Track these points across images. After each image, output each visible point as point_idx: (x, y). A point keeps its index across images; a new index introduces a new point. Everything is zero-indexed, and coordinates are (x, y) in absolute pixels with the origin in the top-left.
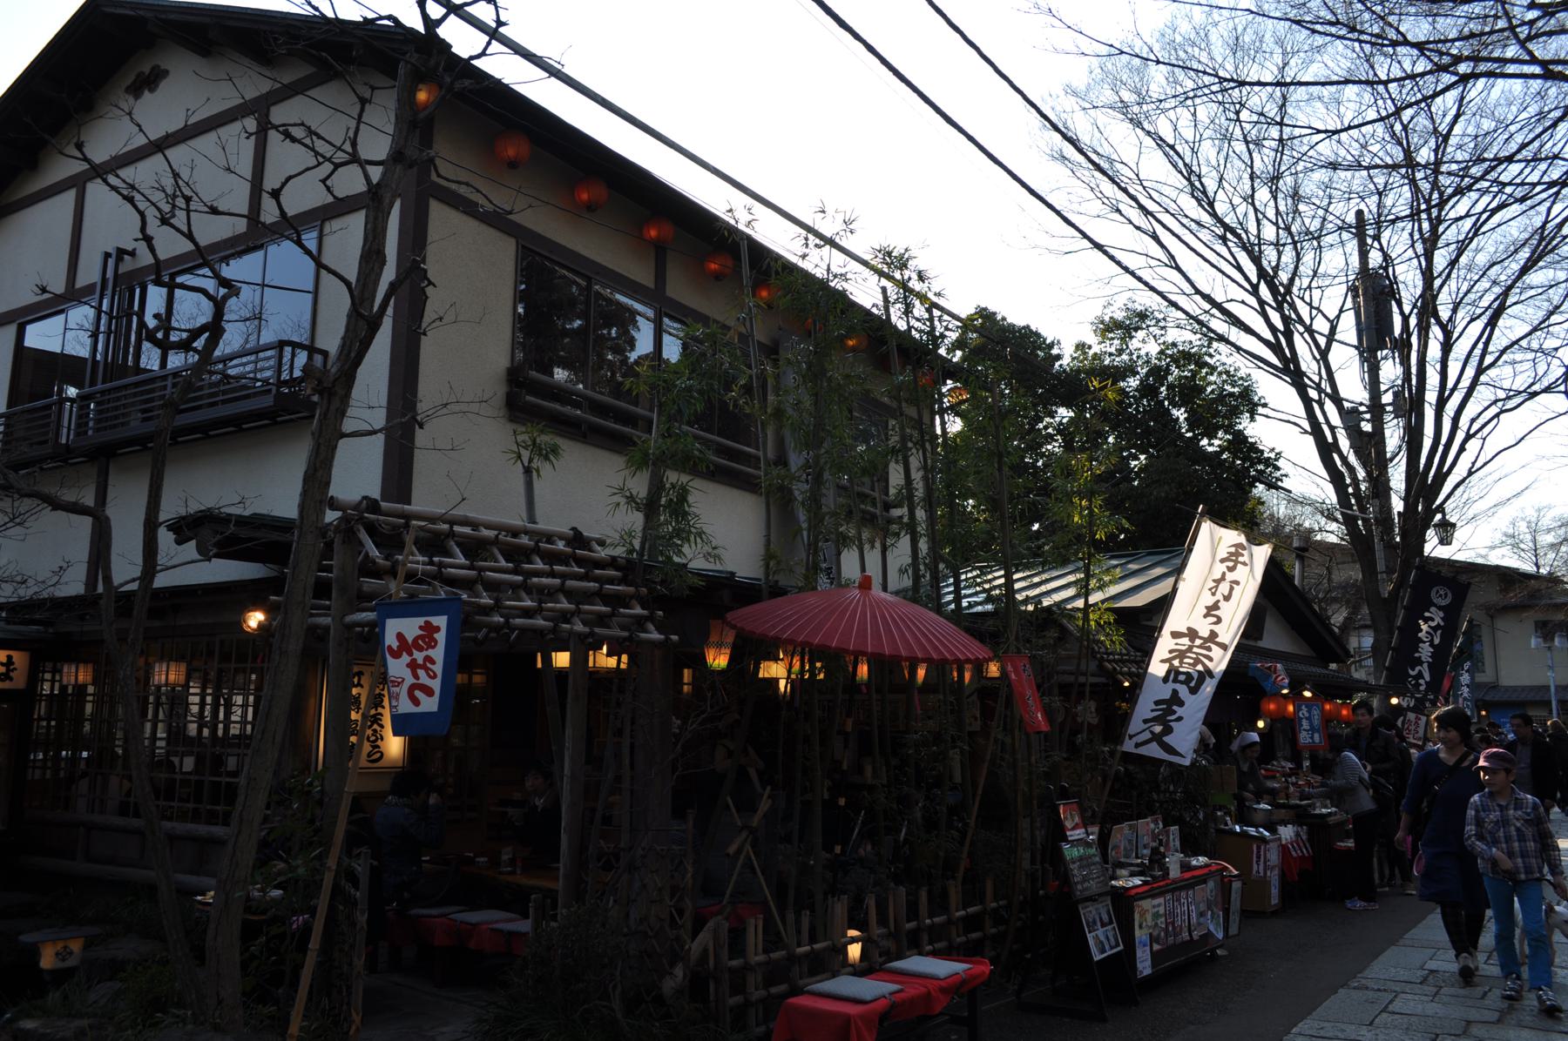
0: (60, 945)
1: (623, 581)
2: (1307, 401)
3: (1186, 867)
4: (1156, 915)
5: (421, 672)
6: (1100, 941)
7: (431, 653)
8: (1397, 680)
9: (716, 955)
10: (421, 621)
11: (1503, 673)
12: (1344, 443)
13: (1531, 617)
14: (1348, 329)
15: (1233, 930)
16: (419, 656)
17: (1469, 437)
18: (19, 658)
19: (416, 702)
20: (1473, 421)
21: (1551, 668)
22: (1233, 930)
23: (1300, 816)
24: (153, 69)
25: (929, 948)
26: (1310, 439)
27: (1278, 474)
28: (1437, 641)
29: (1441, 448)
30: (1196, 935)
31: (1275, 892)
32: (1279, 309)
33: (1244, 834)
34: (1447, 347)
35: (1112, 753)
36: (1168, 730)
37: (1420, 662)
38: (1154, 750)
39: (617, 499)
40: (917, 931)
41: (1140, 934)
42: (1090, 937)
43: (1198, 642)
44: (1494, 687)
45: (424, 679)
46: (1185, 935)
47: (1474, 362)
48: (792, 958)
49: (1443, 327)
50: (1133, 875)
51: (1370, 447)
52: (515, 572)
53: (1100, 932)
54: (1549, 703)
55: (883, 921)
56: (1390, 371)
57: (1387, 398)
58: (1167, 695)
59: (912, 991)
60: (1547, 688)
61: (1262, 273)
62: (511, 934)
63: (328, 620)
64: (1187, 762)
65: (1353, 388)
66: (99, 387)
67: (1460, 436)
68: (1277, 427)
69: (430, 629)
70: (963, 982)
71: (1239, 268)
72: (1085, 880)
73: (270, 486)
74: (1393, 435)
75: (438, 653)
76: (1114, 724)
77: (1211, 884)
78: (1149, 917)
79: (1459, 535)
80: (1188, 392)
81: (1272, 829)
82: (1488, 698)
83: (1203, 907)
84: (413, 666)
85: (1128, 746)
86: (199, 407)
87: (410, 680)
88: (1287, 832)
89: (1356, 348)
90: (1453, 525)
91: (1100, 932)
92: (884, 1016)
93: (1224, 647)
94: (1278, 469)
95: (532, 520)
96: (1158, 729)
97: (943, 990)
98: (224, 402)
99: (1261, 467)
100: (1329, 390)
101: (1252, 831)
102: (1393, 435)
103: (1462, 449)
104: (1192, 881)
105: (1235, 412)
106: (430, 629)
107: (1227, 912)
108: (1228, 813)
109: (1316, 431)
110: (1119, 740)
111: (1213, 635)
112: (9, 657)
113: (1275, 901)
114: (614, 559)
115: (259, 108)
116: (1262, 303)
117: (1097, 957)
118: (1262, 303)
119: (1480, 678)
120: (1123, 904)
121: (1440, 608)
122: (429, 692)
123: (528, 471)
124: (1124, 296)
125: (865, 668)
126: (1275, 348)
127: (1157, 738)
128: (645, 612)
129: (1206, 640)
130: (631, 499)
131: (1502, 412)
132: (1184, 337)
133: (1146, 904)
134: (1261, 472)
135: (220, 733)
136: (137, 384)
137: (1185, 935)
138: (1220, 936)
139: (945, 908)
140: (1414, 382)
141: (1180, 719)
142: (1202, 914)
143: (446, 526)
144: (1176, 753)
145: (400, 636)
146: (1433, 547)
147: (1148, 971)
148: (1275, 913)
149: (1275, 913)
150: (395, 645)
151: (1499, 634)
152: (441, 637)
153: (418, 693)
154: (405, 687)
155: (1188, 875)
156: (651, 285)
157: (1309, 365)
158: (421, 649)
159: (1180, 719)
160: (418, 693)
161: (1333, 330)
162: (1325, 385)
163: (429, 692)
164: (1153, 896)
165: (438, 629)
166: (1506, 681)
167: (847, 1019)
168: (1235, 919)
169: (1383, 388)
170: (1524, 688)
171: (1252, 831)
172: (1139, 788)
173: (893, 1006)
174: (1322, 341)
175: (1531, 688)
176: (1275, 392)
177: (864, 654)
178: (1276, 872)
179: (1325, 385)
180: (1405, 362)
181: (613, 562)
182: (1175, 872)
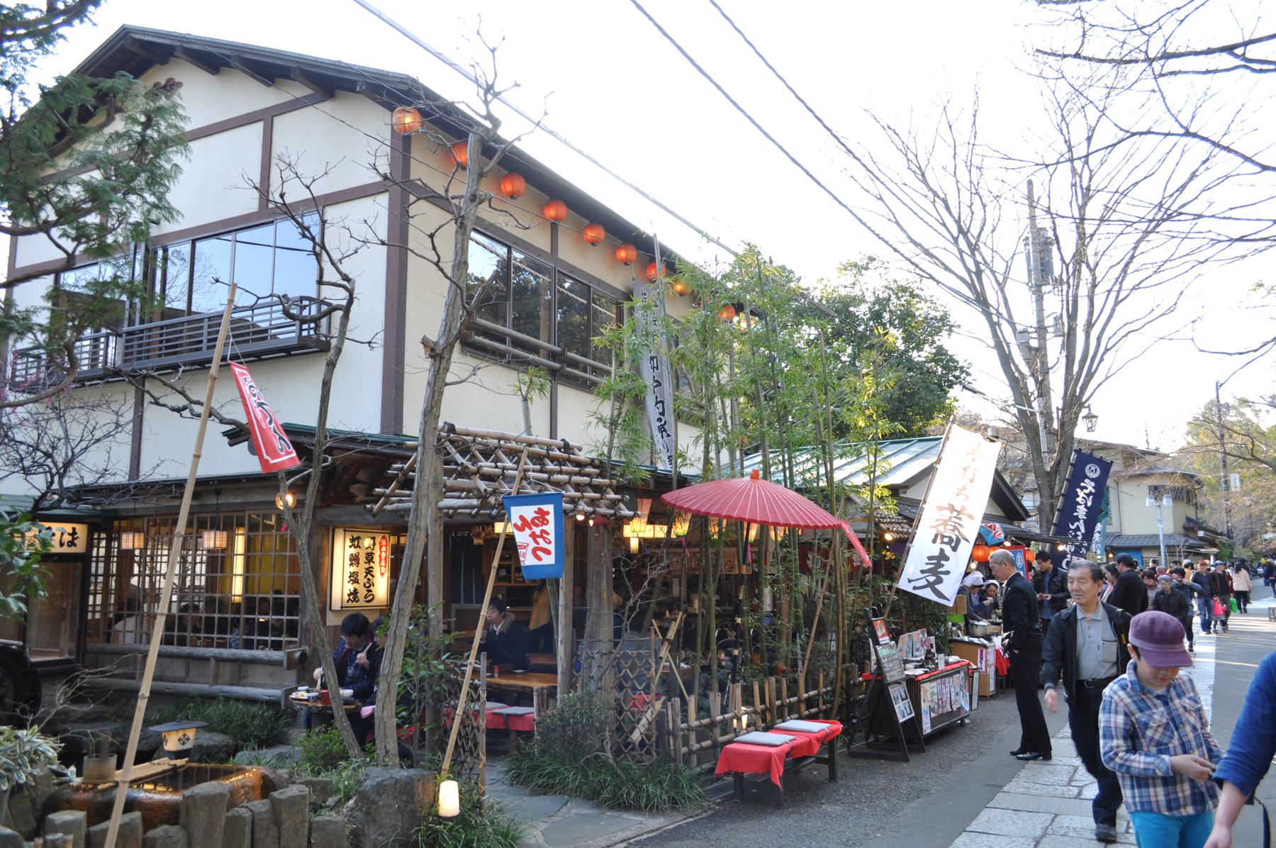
0: (181, 734)
1: (601, 475)
2: (994, 326)
3: (947, 663)
4: (932, 694)
5: (540, 540)
6: (902, 710)
7: (544, 527)
9: (674, 721)
10: (535, 508)
14: (1020, 270)
15: (975, 706)
16: (537, 530)
18: (81, 530)
19: (540, 559)
21: (1160, 521)
24: (168, 80)
25: (806, 713)
26: (995, 352)
28: (1089, 504)
31: (992, 682)
32: (973, 255)
35: (890, 588)
37: (1077, 519)
39: (591, 419)
40: (782, 705)
41: (924, 706)
45: (542, 544)
47: (1113, 295)
49: (1092, 271)
51: (1036, 355)
52: (541, 471)
54: (1159, 547)
55: (763, 701)
59: (801, 740)
61: (961, 230)
62: (508, 715)
63: (410, 504)
65: (1025, 316)
66: (137, 326)
68: (968, 342)
69: (542, 514)
70: (828, 735)
71: (944, 224)
73: (288, 400)
74: (1054, 347)
75: (550, 528)
76: (892, 569)
77: (962, 674)
79: (1099, 424)
80: (905, 318)
81: (989, 639)
82: (1114, 544)
83: (958, 689)
84: (533, 536)
85: (903, 584)
86: (247, 341)
87: (532, 545)
92: (788, 754)
95: (530, 434)
97: (818, 739)
98: (254, 340)
99: (957, 373)
100: (1005, 315)
101: (976, 640)
102: (1054, 347)
103: (1102, 360)
105: (938, 331)
106: (542, 514)
107: (971, 697)
108: (959, 628)
110: (895, 579)
112: (74, 529)
113: (992, 688)
114: (593, 460)
115: (266, 117)
116: (961, 251)
117: (901, 720)
118: (961, 251)
119: (1109, 529)
120: (913, 686)
121: (1092, 480)
122: (548, 552)
123: (525, 399)
124: (860, 245)
126: (971, 286)
130: (600, 419)
132: (904, 276)
134: (957, 378)
135: (188, 583)
136: (190, 322)
138: (967, 708)
142: (957, 694)
143: (496, 441)
145: (522, 518)
146: (1081, 432)
149: (992, 697)
150: (519, 523)
151: (1123, 496)
152: (551, 518)
153: (539, 553)
155: (949, 667)
156: (549, 250)
157: (992, 297)
158: (537, 526)
160: (539, 553)
161: (1008, 268)
162: (1003, 310)
163: (548, 552)
165: (548, 513)
166: (1128, 530)
167: (770, 756)
168: (975, 698)
169: (1046, 314)
170: (1140, 537)
171: (976, 640)
172: (915, 613)
173: (792, 748)
174: (1000, 279)
176: (968, 318)
177: (755, 521)
178: (993, 668)
179: (1003, 310)
181: (592, 463)
182: (942, 667)
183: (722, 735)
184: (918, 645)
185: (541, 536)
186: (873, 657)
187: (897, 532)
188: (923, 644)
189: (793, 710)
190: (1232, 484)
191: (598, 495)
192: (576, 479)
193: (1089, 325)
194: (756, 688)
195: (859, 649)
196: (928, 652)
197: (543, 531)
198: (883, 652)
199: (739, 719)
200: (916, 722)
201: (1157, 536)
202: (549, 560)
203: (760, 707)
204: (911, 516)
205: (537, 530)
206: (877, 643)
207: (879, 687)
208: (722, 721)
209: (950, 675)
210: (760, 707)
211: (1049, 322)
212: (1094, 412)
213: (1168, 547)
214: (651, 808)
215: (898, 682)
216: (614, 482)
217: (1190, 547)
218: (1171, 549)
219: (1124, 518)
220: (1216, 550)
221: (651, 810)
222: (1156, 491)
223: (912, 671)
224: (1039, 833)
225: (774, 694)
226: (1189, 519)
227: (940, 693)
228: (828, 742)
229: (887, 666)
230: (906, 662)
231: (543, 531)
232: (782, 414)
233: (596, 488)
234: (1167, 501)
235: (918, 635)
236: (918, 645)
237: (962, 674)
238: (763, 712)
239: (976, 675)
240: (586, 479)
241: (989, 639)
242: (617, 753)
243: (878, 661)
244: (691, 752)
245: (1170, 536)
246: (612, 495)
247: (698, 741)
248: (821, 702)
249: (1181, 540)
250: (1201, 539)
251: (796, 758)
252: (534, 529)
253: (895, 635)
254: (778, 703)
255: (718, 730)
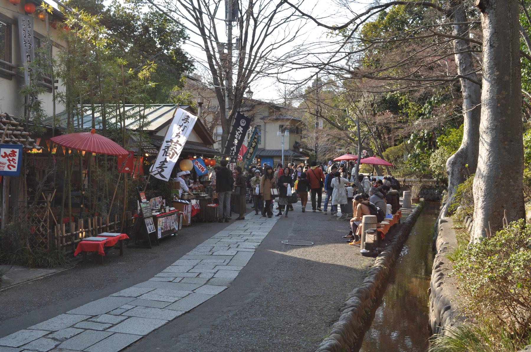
2: (206, 42)
3: (170, 210)
4: (163, 223)
5: (11, 162)
6: (150, 228)
7: (14, 158)
8: (228, 152)
9: (57, 233)
10: (11, 150)
11: (267, 145)
12: (218, 56)
13: (279, 123)
14: (221, 13)
16: (11, 158)
17: (261, 58)
19: (10, 169)
20: (263, 52)
22: (180, 228)
23: (197, 197)
26: (205, 52)
27: (192, 68)
29: (251, 64)
30: (172, 228)
31: (189, 219)
33: (181, 202)
34: (255, 27)
36: (163, 171)
38: (158, 177)
40: (100, 228)
41: (159, 227)
42: (147, 227)
43: (173, 144)
44: (263, 150)
45: (12, 163)
46: (169, 228)
48: (72, 235)
50: (156, 212)
51: (226, 59)
53: (150, 226)
54: (281, 156)
55: (92, 226)
56: (236, 31)
57: (234, 41)
58: (164, 160)
60: (281, 151)
64: (167, 180)
67: (256, 62)
68: (193, 48)
69: (14, 153)
72: (146, 213)
74: (235, 53)
75: (17, 158)
77: (176, 215)
78: (161, 223)
80: (161, 31)
81: (189, 201)
82: (261, 154)
83: (173, 221)
84: (9, 160)
88: (194, 202)
89: (225, 21)
90: (252, 93)
91: (150, 226)
92: (105, 244)
93: (181, 145)
94: (193, 66)
96: (160, 170)
100: (213, 33)
101: (183, 201)
104: (171, 214)
106: (14, 153)
109: (207, 50)
111: (178, 141)
113: (189, 222)
117: (149, 233)
120: (155, 218)
121: (242, 127)
122: (14, 167)
125: (55, 150)
127: (159, 173)
128: (33, 140)
129: (175, 143)
131: (273, 49)
133: (160, 219)
137: (169, 228)
138: (177, 229)
139: (114, 221)
140: (243, 40)
141: (166, 167)
142: (173, 223)
144: (165, 178)
145: (5, 153)
147: (160, 237)
148: (189, 226)
149: (189, 226)
150: (4, 155)
152: (17, 154)
153: (10, 167)
154: (6, 165)
158: (11, 156)
159: (166, 167)
160: (10, 167)
163: (14, 167)
164: (162, 217)
165: (16, 152)
166: (268, 148)
169: (233, 37)
170: (273, 151)
171: (183, 201)
175: (276, 151)
179: (212, 31)
180: (241, 27)
182: (167, 211)
183: (76, 239)
184: (158, 203)
185: (12, 161)
186: (139, 208)
187: (151, 153)
188: (160, 202)
189: (105, 230)
190: (320, 125)
191: (25, 140)
192: (15, 132)
193: (252, 47)
194: (90, 221)
195: (133, 205)
196: (162, 206)
197: (13, 159)
198: (143, 205)
199: (82, 234)
200: (156, 233)
201: (281, 151)
202: (14, 170)
203: (91, 229)
204: (158, 145)
205: (11, 158)
206: (140, 202)
207: (141, 219)
208: (75, 234)
209: (171, 215)
210: (91, 229)
211: (234, 41)
212: (252, 90)
213: (285, 156)
214: (50, 267)
215: (148, 217)
216: (31, 133)
217: (295, 156)
218: (287, 158)
219: (267, 142)
220: (308, 158)
221: (50, 267)
222: (282, 129)
223: (155, 213)
224: (195, 264)
225: (97, 223)
226: (296, 143)
227: (166, 222)
228: (120, 240)
229: (144, 211)
230: (153, 210)
231: (13, 159)
232: (90, 83)
233: (24, 136)
234: (287, 133)
235: (158, 199)
236: (158, 203)
237: (176, 215)
238: (92, 231)
239: (181, 215)
240: (19, 132)
241: (189, 201)
242: (32, 247)
243: (141, 210)
244: (63, 246)
245: (287, 151)
246: (30, 140)
247: (66, 242)
248: (116, 227)
249: (291, 153)
250: (301, 153)
251: (107, 246)
252: (10, 158)
253: (148, 198)
254: (98, 227)
255: (74, 238)
